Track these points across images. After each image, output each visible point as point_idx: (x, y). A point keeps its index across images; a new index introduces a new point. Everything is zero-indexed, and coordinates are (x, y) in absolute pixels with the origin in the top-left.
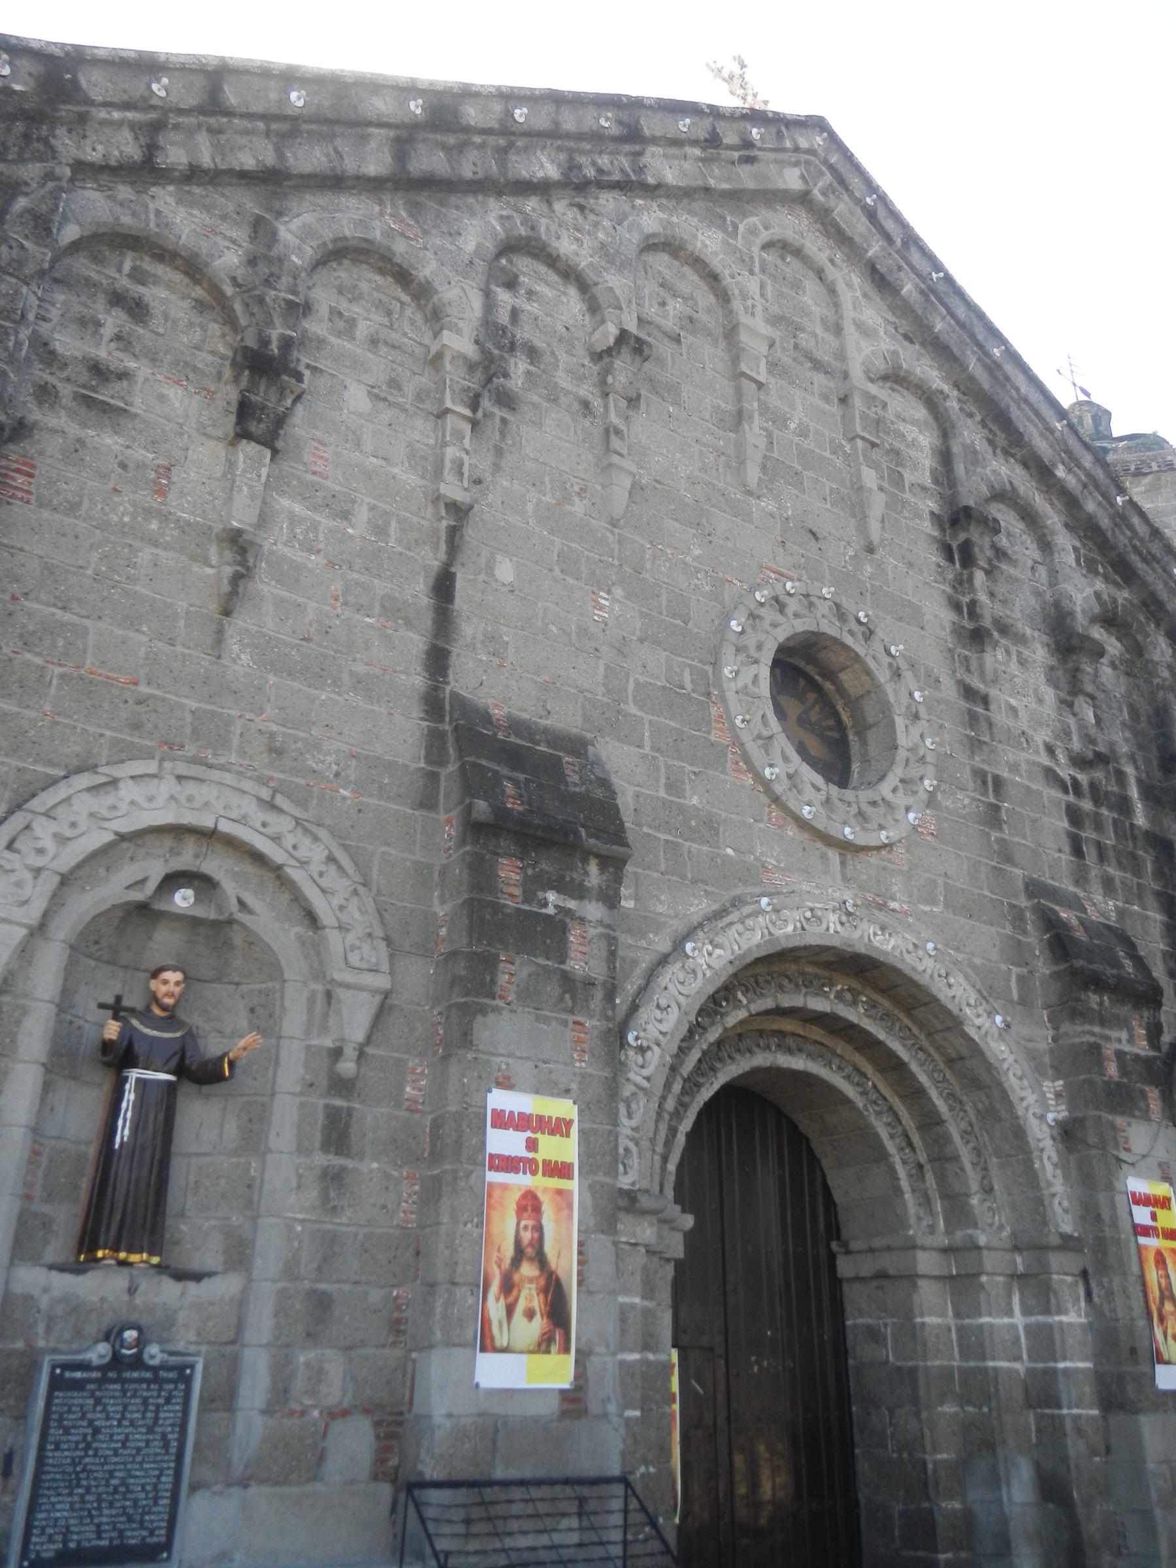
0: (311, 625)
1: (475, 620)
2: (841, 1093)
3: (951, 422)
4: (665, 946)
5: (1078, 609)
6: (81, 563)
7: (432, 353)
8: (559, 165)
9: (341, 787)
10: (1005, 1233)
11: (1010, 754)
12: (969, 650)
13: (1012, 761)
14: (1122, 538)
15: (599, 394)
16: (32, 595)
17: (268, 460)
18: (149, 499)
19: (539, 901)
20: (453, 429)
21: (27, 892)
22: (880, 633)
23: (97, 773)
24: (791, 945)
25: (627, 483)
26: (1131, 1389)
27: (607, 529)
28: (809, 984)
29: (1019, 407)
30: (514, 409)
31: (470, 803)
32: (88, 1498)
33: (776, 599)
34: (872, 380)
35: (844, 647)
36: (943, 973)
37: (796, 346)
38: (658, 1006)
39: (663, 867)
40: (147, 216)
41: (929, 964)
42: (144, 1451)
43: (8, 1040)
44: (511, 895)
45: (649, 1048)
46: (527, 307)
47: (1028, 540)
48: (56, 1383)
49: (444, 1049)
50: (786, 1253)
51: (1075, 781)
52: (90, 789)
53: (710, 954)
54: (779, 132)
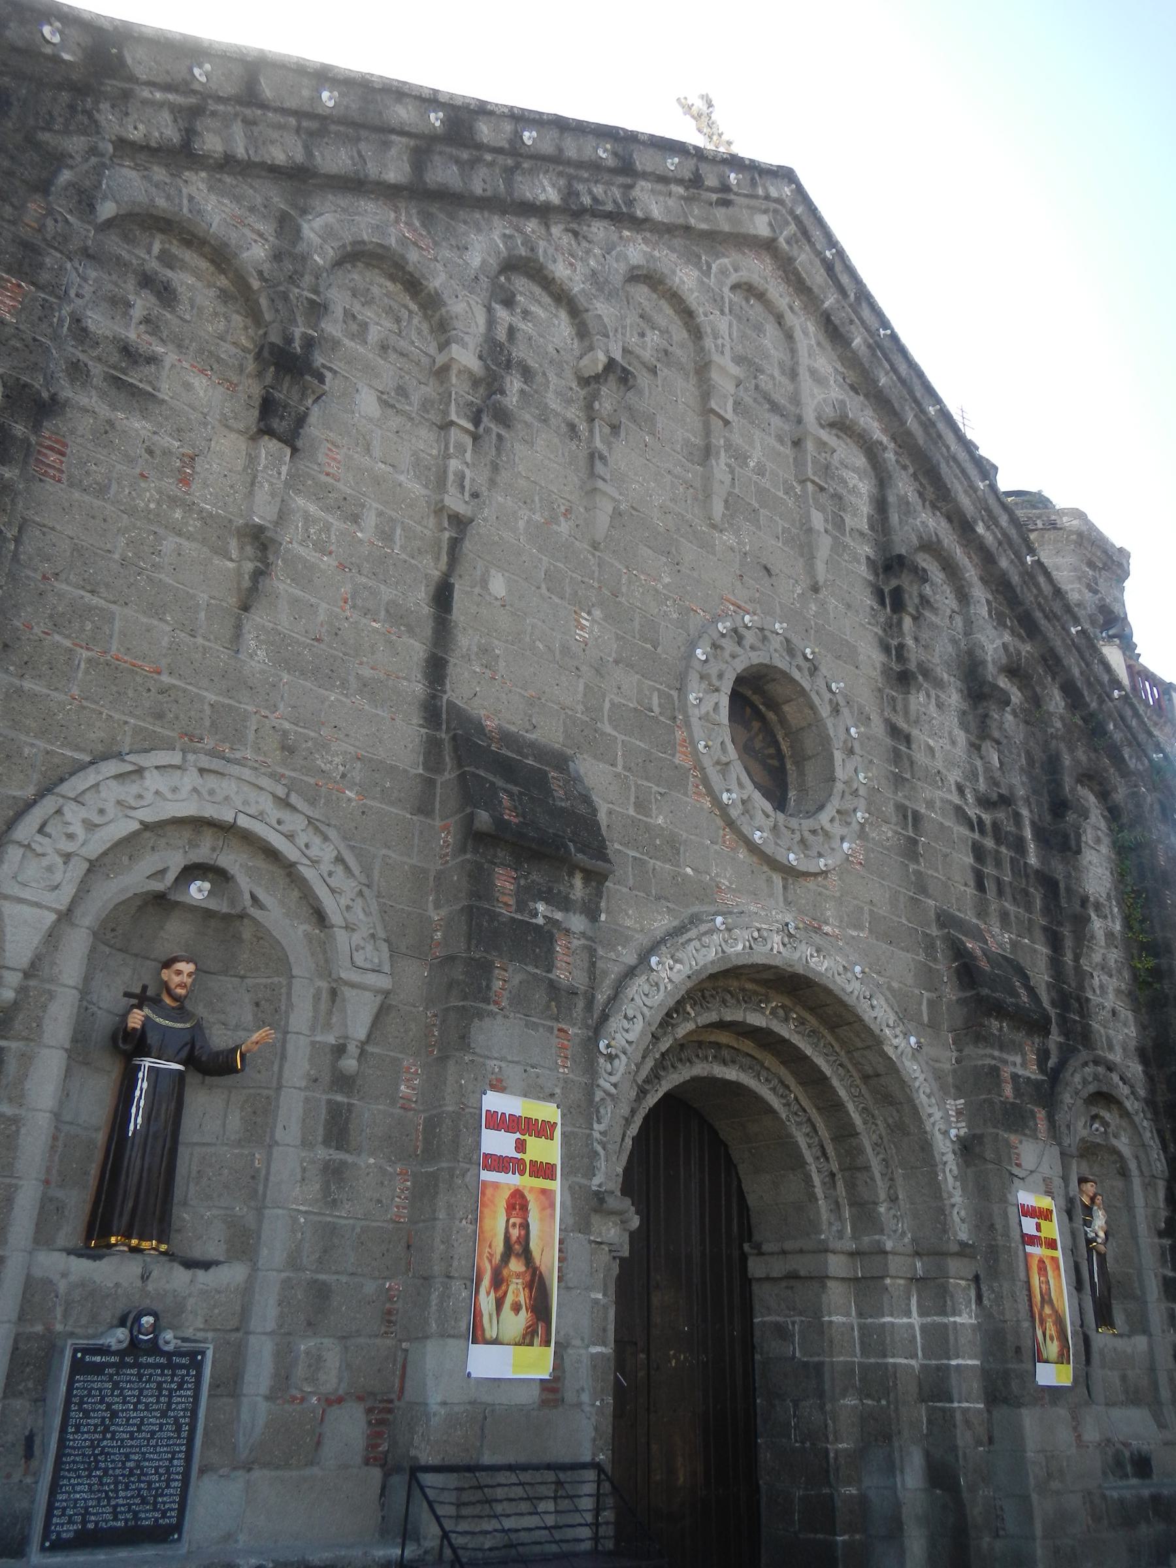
0: (322, 625)
1: (470, 631)
2: (767, 1103)
3: (888, 472)
4: (629, 957)
5: (989, 659)
6: (109, 546)
8: (559, 190)
10: (907, 1239)
13: (928, 798)
16: (63, 576)
17: (288, 458)
18: (173, 487)
19: (531, 911)
20: (456, 442)
21: (58, 877)
22: (823, 670)
23: (124, 761)
24: (740, 963)
25: (609, 508)
26: (1015, 1386)
27: (589, 552)
28: (747, 999)
30: (509, 426)
31: (472, 814)
33: (735, 631)
34: (822, 426)
35: (793, 681)
36: (868, 994)
37: (757, 387)
38: (626, 1017)
39: (631, 883)
40: (181, 201)
43: (34, 1025)
44: (506, 904)
45: (617, 1056)
46: (522, 326)
47: (947, 589)
48: (77, 1367)
49: (439, 1050)
51: (980, 821)
52: (119, 777)
53: (671, 969)
54: (753, 179)
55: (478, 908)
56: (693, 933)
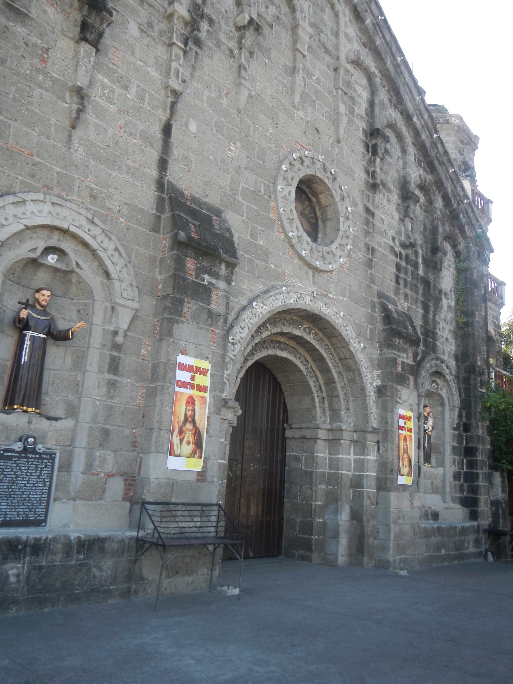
1: (179, 148)
2: (299, 368)
4: (245, 303)
5: (412, 181)
6: (7, 91)
7: (168, 13)
9: (121, 217)
11: (379, 239)
12: (370, 192)
13: (379, 241)
14: (433, 152)
15: (237, 47)
17: (94, 54)
18: (38, 64)
22: (339, 180)
24: (292, 308)
25: (246, 93)
26: (389, 484)
27: (236, 114)
28: (293, 323)
29: (404, 86)
30: (201, 48)
31: (177, 232)
32: (14, 501)
33: (301, 158)
34: (348, 62)
35: (324, 183)
37: (319, 40)
38: (241, 327)
41: (340, 320)
42: (36, 485)
45: (236, 343)
47: (397, 147)
49: (159, 336)
50: (267, 427)
51: (400, 254)
53: (262, 308)
55: (178, 275)
56: (272, 293)
